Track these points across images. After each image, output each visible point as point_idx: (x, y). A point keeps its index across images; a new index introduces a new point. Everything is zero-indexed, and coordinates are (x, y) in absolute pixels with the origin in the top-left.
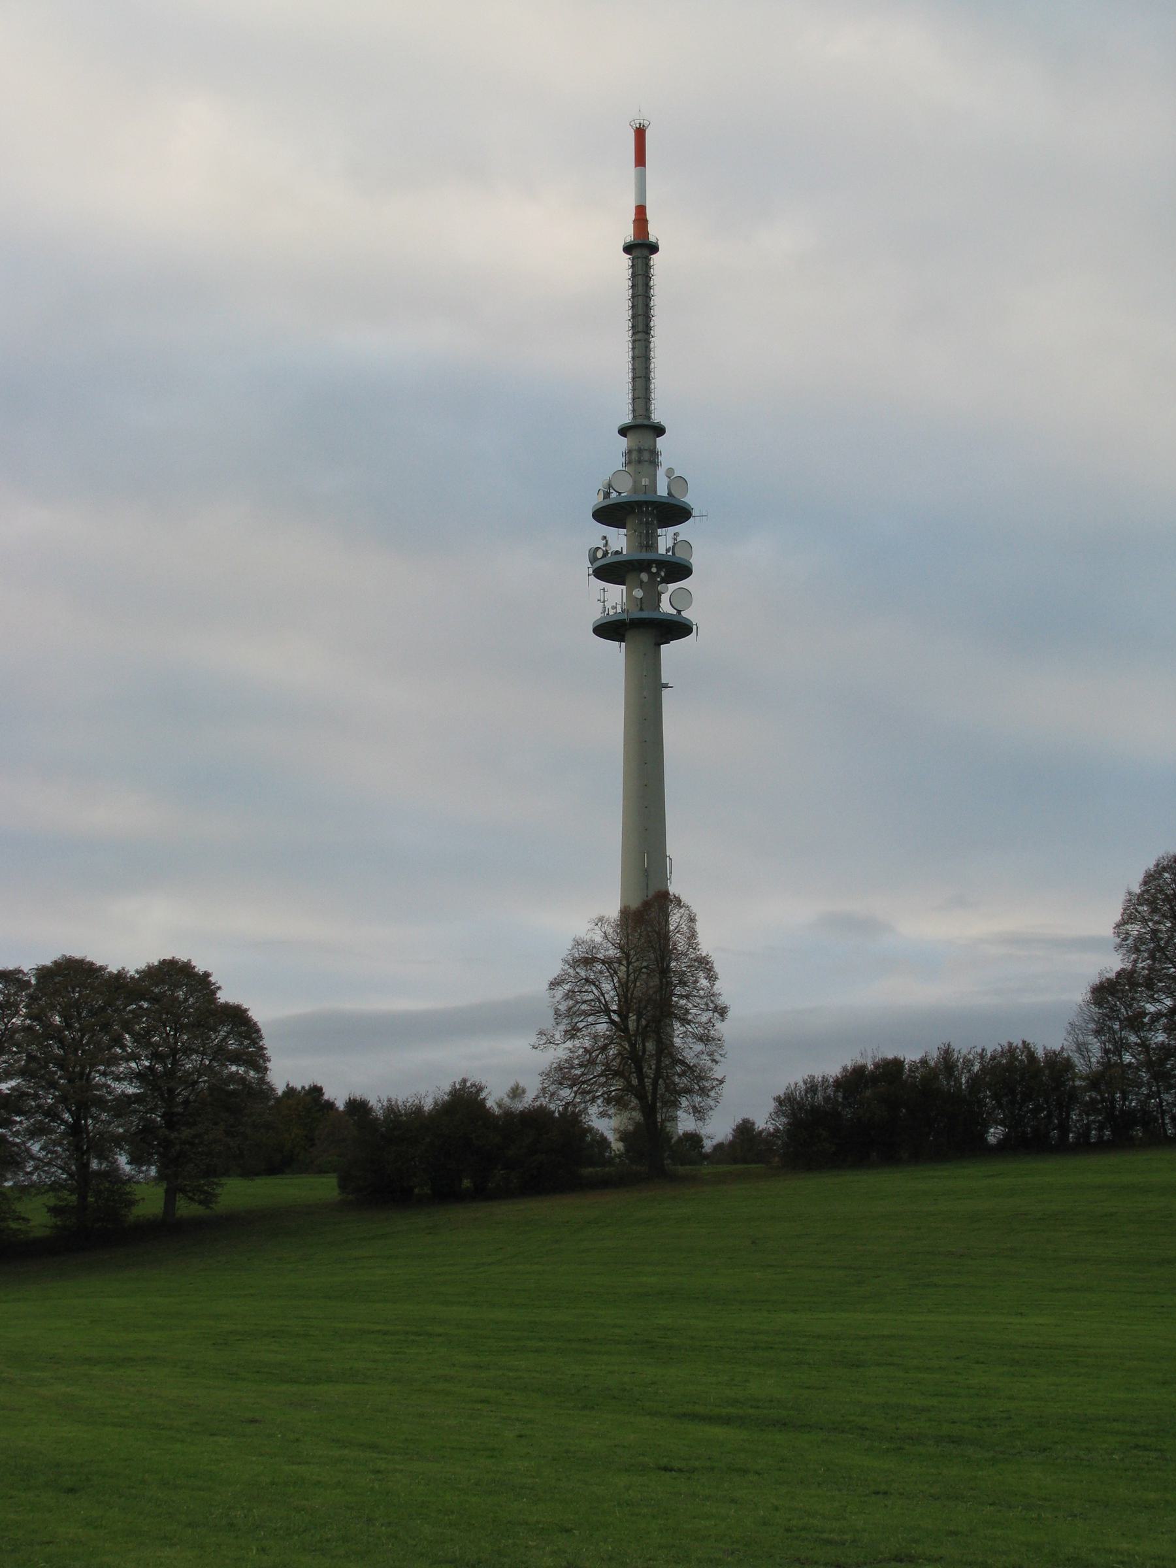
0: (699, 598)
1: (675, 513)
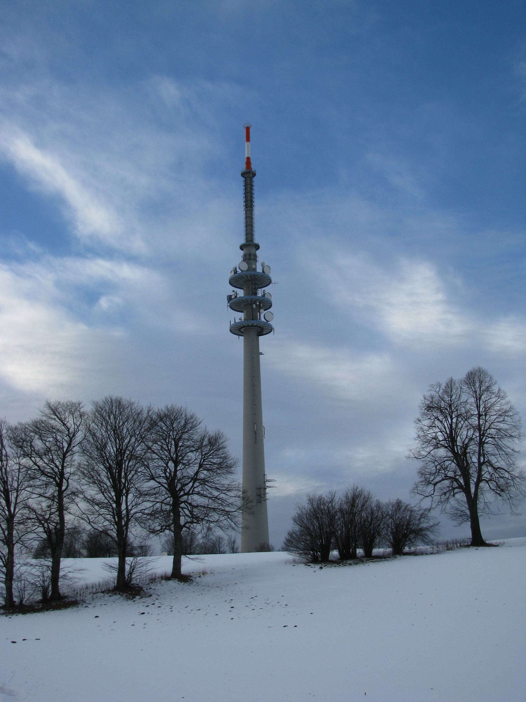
0: (275, 316)
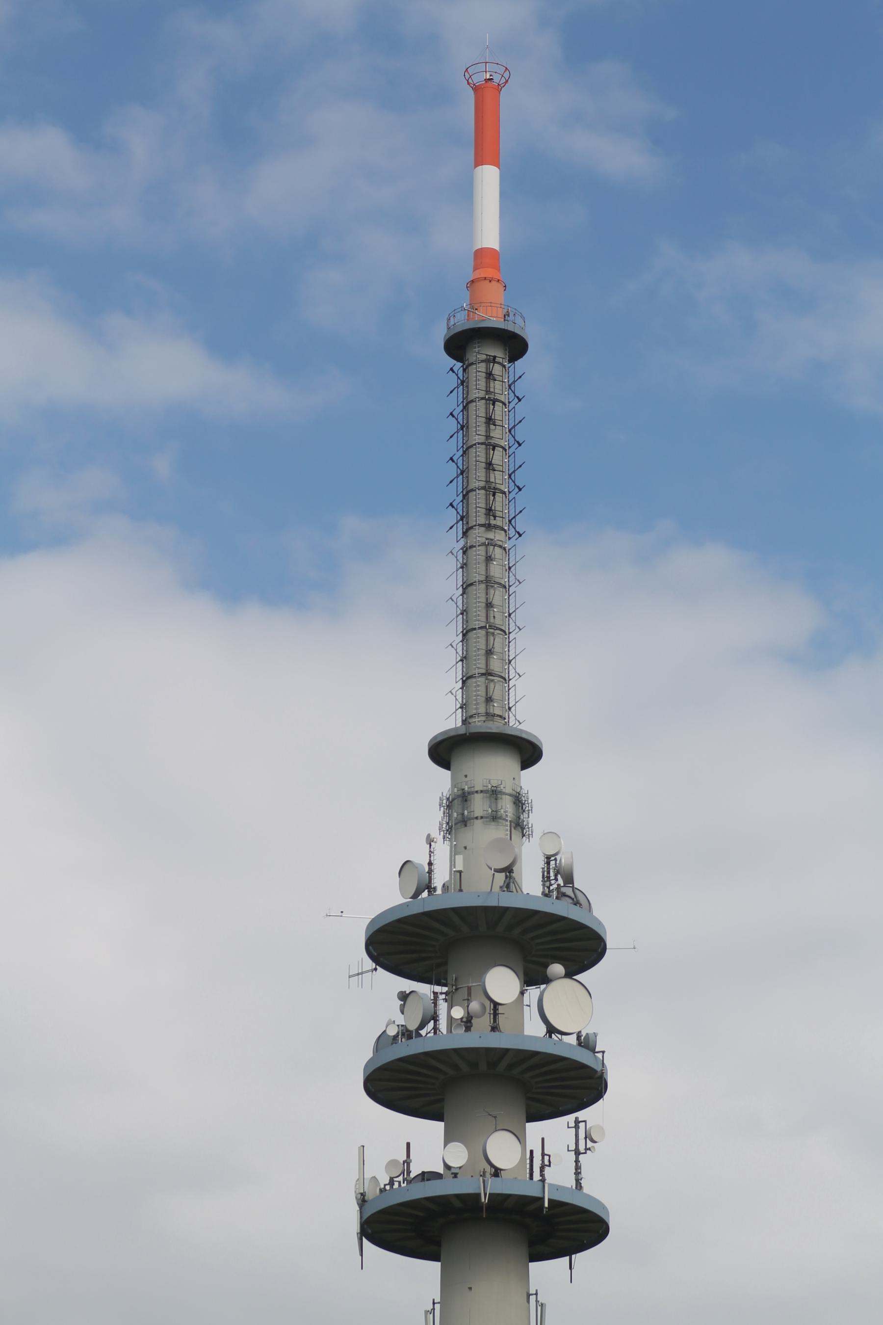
1: (560, 943)
